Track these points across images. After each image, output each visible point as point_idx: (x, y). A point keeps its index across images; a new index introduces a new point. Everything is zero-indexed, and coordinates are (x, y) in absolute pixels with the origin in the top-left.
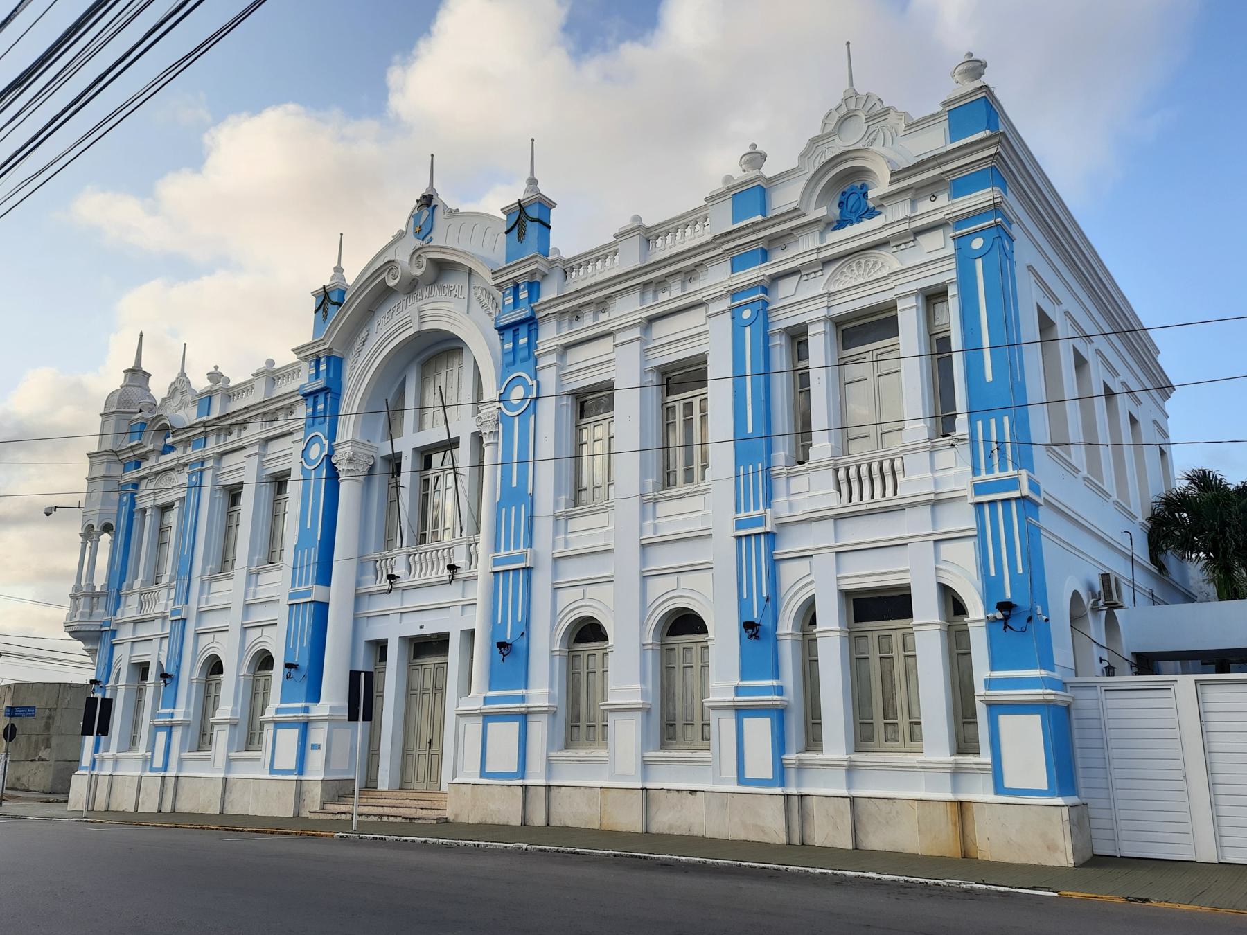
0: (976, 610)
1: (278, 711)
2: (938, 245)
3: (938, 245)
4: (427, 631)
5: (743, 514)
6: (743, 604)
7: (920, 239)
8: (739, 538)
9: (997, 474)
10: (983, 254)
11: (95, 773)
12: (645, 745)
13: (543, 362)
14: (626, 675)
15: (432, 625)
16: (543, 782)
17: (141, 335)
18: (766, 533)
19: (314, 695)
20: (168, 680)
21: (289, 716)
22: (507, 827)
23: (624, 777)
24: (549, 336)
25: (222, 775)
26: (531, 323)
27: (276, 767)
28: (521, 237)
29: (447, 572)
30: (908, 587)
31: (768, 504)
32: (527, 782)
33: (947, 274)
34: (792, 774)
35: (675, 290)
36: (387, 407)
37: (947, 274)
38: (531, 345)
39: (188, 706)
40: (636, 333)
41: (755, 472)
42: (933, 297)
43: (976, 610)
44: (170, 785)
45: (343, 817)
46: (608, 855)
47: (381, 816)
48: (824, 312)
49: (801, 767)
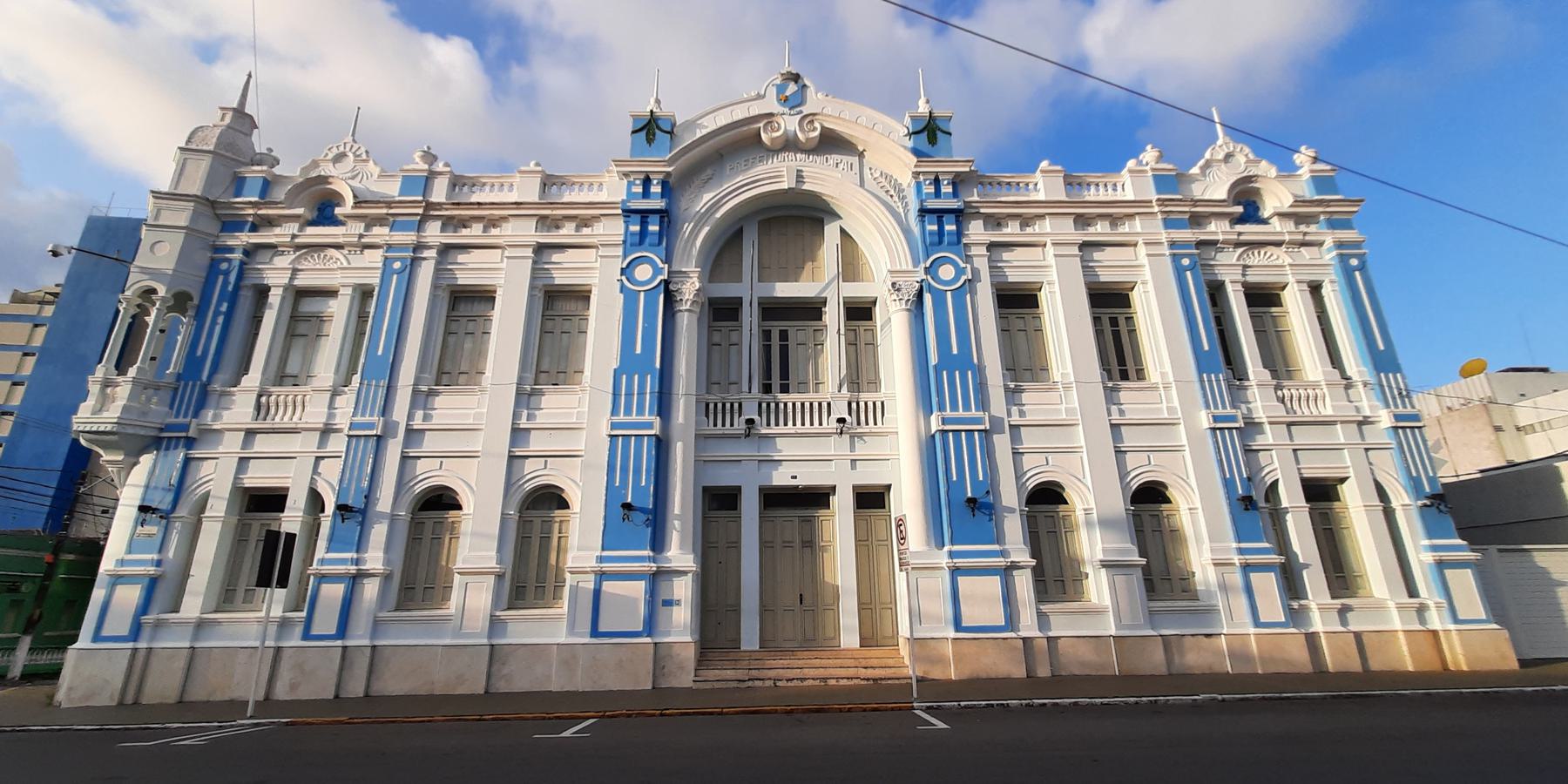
0: (330, 508)
1: (122, 562)
2: (375, 258)
3: (375, 258)
4: (801, 482)
5: (621, 418)
6: (1228, 484)
7: (366, 251)
8: (611, 436)
9: (634, 418)
10: (399, 272)
11: (142, 645)
12: (496, 604)
13: (974, 251)
14: (477, 543)
15: (808, 477)
16: (366, 642)
17: (250, 76)
18: (187, 438)
19: (658, 543)
20: (347, 515)
21: (341, 569)
22: (1152, 678)
23: (361, 637)
24: (976, 231)
25: (187, 645)
26: (960, 215)
27: (602, 629)
28: (650, 141)
29: (835, 425)
30: (287, 489)
31: (196, 415)
32: (349, 643)
33: (374, 279)
34: (146, 632)
35: (477, 229)
36: (725, 249)
37: (376, 281)
38: (960, 233)
39: (387, 550)
40: (529, 252)
41: (377, 386)
42: (364, 293)
43: (330, 508)
44: (140, 657)
45: (758, 683)
46: (1324, 698)
47: (825, 679)
48: (1240, 278)
49: (159, 625)
